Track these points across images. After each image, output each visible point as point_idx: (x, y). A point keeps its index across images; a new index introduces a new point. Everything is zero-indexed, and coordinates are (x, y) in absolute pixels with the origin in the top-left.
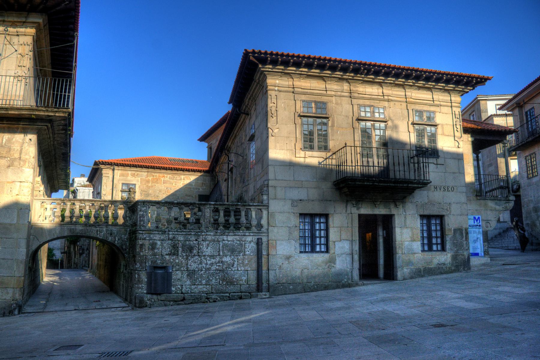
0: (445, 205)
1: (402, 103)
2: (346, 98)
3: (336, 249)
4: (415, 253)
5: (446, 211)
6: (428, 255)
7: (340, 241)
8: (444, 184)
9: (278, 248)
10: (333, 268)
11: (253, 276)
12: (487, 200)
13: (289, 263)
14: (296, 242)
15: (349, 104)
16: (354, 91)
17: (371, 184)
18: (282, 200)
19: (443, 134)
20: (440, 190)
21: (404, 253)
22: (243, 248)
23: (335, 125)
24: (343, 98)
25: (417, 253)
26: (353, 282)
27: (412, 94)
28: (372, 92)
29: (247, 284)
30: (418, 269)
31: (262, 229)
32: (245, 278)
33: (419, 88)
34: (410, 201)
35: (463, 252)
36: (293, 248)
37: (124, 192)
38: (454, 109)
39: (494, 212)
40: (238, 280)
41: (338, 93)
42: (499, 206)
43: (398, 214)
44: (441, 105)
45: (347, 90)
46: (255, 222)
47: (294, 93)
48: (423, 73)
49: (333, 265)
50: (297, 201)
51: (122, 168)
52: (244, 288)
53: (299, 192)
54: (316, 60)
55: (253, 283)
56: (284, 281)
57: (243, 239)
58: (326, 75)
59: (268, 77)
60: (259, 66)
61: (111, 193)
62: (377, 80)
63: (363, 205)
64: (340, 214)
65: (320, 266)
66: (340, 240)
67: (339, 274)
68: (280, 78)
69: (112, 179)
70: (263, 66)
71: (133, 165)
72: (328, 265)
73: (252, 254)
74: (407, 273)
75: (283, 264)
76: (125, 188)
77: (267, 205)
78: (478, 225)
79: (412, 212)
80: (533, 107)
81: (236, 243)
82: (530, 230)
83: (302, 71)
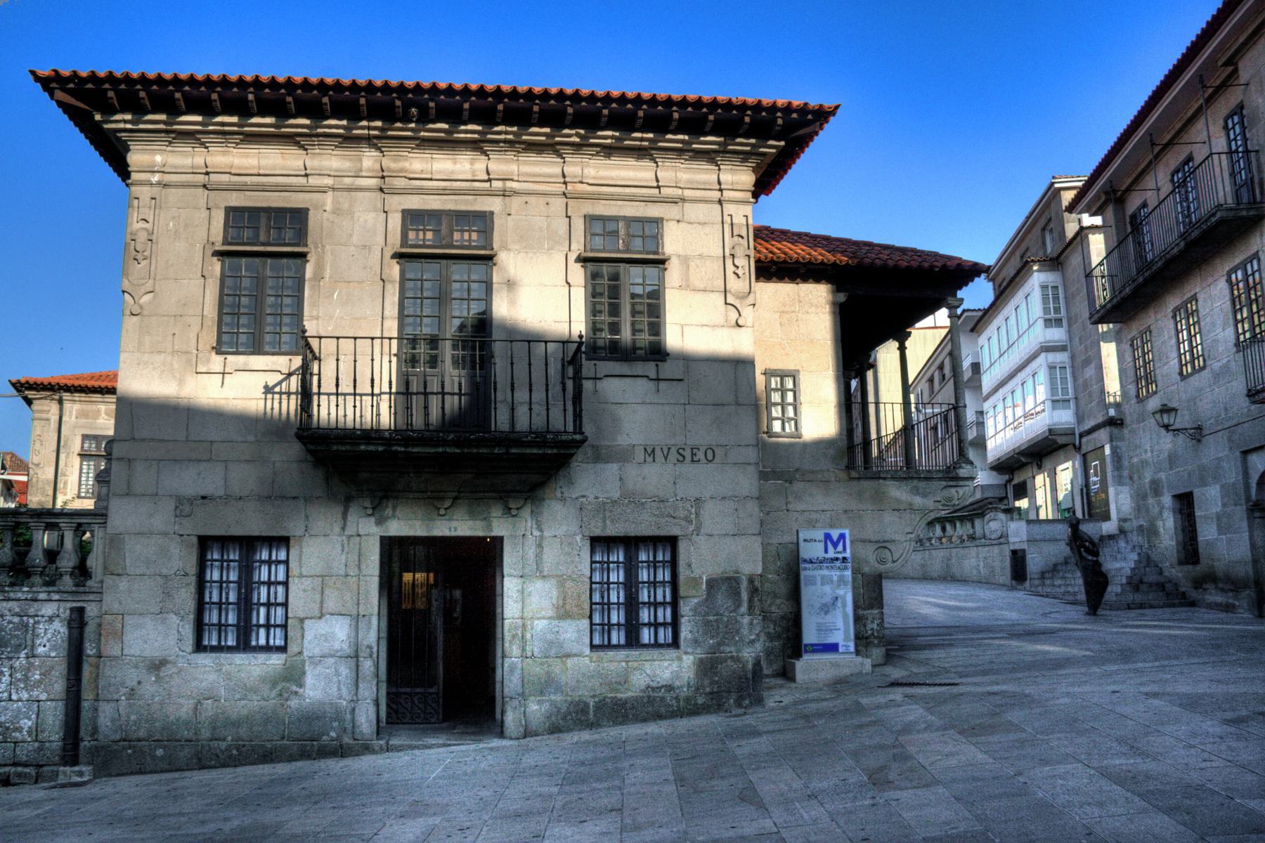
0: (680, 504)
1: (552, 200)
2: (367, 194)
3: (306, 641)
4: (568, 656)
5: (683, 523)
6: (614, 662)
7: (320, 618)
8: (679, 440)
9: (128, 637)
10: (292, 697)
11: (54, 715)
12: (884, 479)
13: (159, 679)
14: (182, 619)
15: (375, 210)
16: (394, 172)
17: (381, 449)
18: (147, 498)
19: (686, 286)
20: (666, 458)
21: (529, 654)
22: (29, 636)
23: (327, 273)
24: (360, 194)
25: (576, 655)
26: (355, 739)
27: (586, 171)
28: (453, 172)
29: (36, 740)
30: (578, 703)
31: (89, 583)
32: (30, 723)
33: (608, 151)
34: (559, 495)
35: (739, 651)
36: (172, 640)
37: (87, 458)
38: (729, 208)
39: (907, 515)
40: (8, 729)
41: (346, 179)
42: (924, 495)
43: (514, 537)
44: (683, 200)
45: (373, 171)
46: (69, 560)
47: (207, 189)
48: (599, 104)
49: (294, 688)
50: (191, 501)
51: (83, 397)
52: (25, 752)
53: (199, 474)
54: (251, 89)
55: (51, 739)
56: (142, 733)
57: (32, 611)
58: (299, 130)
59: (133, 146)
60: (93, 116)
61: (54, 459)
62: (426, 134)
63: (398, 510)
64: (322, 538)
65: (254, 690)
66: (317, 613)
67: (312, 717)
68: (169, 148)
69: (57, 426)
70: (106, 118)
71: (107, 387)
72: (279, 688)
73: (53, 654)
74: (538, 715)
75: (139, 683)
76: (91, 447)
77: (104, 512)
78: (837, 559)
79: (562, 530)
80: (1146, 200)
81: (10, 622)
82: (1146, 545)
83: (223, 124)
